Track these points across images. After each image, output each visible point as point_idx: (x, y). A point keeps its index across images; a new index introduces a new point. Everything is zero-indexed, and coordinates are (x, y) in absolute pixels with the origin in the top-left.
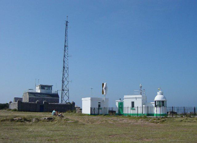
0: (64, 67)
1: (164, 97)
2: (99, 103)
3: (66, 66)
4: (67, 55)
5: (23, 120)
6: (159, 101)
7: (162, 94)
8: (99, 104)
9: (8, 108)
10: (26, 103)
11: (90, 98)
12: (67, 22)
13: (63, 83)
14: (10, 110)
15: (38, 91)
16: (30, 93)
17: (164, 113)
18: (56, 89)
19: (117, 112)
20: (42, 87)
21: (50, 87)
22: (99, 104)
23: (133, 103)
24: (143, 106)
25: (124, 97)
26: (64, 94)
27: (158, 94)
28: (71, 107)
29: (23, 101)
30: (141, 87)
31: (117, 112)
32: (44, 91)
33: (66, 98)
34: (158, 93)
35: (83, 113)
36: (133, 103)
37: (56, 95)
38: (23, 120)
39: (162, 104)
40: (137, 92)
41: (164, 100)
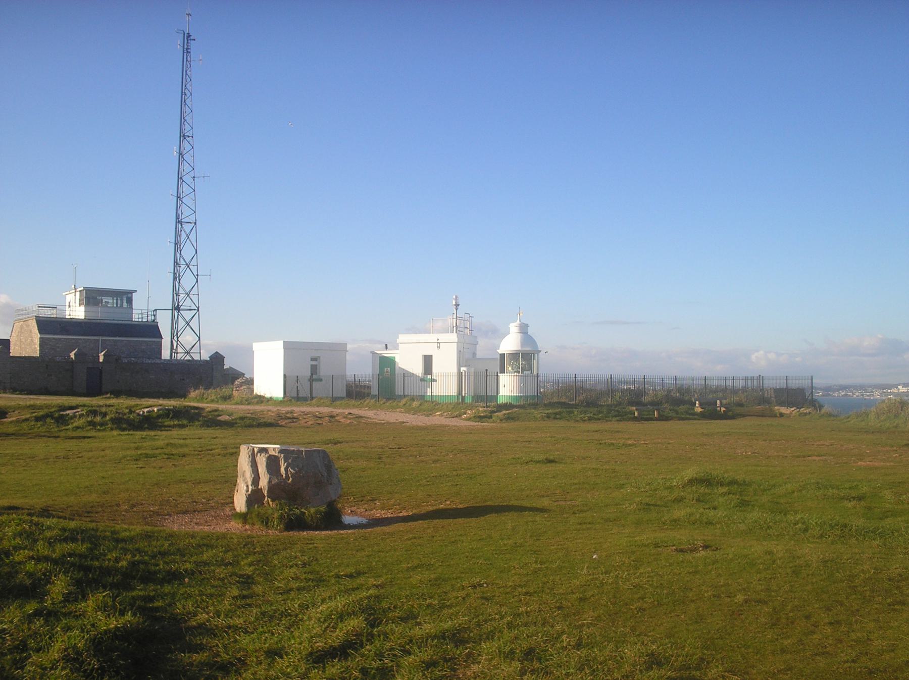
0: (179, 221)
2: (313, 359)
3: (186, 214)
4: (192, 174)
8: (314, 363)
10: (25, 361)
11: (280, 345)
12: (189, 36)
13: (175, 279)
15: (77, 312)
18: (149, 302)
19: (374, 391)
20: (91, 297)
21: (126, 296)
24: (463, 369)
25: (398, 341)
26: (182, 323)
28: (215, 373)
29: (15, 351)
31: (374, 391)
32: (99, 314)
33: (187, 339)
35: (163, 358)
37: (151, 330)
39: (524, 359)
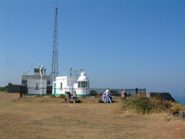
1: (87, 78)
5: (120, 111)
6: (82, 82)
7: (85, 75)
8: (37, 85)
9: (27, 93)
14: (54, 96)
16: (150, 93)
17: (85, 94)
22: (37, 85)
23: (61, 84)
27: (81, 75)
30: (71, 68)
34: (82, 74)
35: (20, 94)
36: (61, 84)
38: (120, 111)
39: (83, 84)
40: (65, 73)
41: (86, 81)
